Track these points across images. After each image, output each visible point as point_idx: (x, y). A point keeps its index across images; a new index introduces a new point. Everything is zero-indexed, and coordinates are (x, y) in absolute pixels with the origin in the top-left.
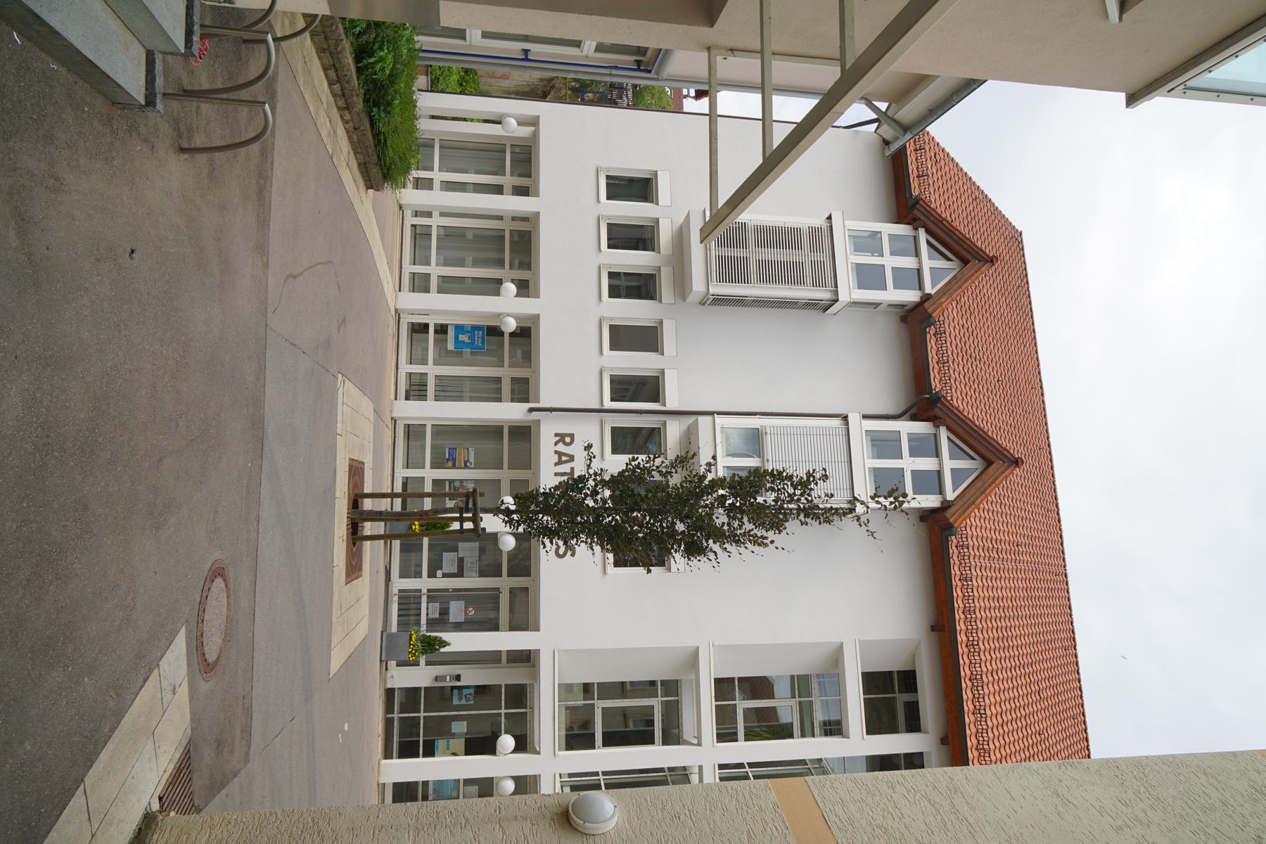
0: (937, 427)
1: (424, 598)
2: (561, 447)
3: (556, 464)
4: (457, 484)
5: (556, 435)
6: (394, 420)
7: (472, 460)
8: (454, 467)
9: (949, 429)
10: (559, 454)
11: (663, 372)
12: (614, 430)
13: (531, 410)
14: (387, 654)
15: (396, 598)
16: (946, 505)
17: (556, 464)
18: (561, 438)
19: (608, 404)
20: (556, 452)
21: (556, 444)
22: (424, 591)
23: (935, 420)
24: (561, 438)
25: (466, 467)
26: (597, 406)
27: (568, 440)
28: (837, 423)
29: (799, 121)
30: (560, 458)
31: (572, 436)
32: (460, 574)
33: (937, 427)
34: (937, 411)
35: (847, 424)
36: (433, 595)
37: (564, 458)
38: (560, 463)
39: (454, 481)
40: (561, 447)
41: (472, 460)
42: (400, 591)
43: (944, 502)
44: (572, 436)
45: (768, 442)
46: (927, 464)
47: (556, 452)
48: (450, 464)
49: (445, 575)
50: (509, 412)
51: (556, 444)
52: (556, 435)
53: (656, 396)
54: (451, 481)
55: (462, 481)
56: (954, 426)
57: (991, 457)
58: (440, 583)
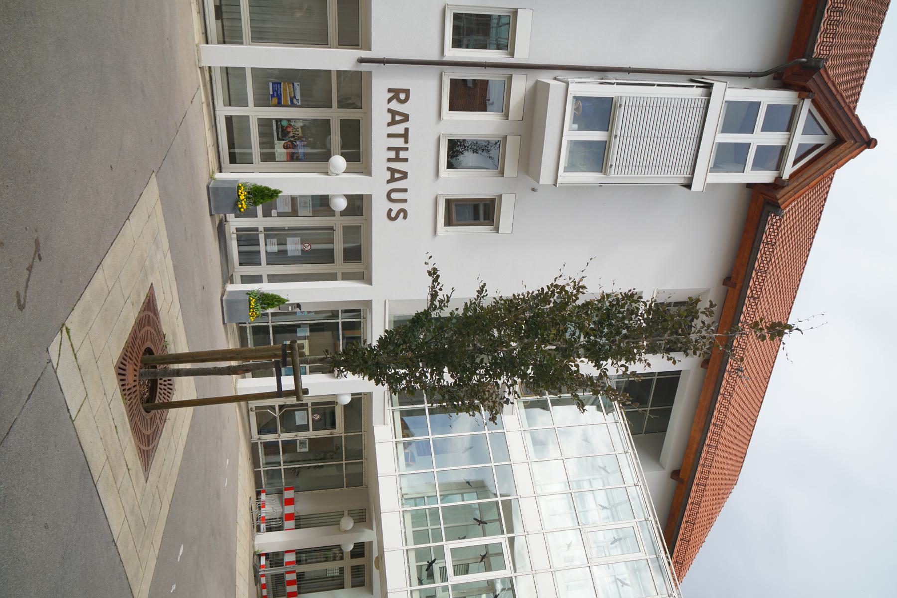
0: (802, 98)
1: (261, 237)
2: (394, 105)
3: (389, 124)
4: (284, 123)
5: (390, 90)
6: (202, 68)
7: (298, 96)
8: (279, 104)
9: (814, 102)
10: (392, 171)
11: (515, 12)
12: (454, 82)
13: (362, 61)
14: (229, 318)
15: (235, 236)
16: (778, 185)
17: (389, 124)
18: (397, 94)
19: (453, 54)
20: (389, 110)
21: (389, 101)
22: (261, 229)
23: (803, 91)
24: (397, 94)
25: (293, 105)
26: (435, 57)
27: (402, 96)
28: (696, 92)
29: (857, 112)
30: (393, 118)
31: (407, 92)
32: (294, 213)
33: (802, 98)
34: (810, 84)
35: (709, 94)
36: (270, 232)
37: (397, 176)
38: (392, 180)
39: (281, 120)
40: (394, 105)
41: (298, 96)
42: (238, 230)
43: (779, 178)
44: (407, 92)
45: (620, 116)
46: (776, 138)
47: (389, 110)
48: (275, 100)
49: (280, 215)
50: (336, 59)
51: (389, 101)
52: (390, 90)
53: (506, 45)
54: (278, 121)
55: (289, 120)
56: (825, 106)
57: (844, 134)
58: (275, 222)
